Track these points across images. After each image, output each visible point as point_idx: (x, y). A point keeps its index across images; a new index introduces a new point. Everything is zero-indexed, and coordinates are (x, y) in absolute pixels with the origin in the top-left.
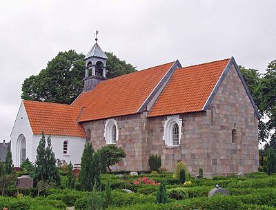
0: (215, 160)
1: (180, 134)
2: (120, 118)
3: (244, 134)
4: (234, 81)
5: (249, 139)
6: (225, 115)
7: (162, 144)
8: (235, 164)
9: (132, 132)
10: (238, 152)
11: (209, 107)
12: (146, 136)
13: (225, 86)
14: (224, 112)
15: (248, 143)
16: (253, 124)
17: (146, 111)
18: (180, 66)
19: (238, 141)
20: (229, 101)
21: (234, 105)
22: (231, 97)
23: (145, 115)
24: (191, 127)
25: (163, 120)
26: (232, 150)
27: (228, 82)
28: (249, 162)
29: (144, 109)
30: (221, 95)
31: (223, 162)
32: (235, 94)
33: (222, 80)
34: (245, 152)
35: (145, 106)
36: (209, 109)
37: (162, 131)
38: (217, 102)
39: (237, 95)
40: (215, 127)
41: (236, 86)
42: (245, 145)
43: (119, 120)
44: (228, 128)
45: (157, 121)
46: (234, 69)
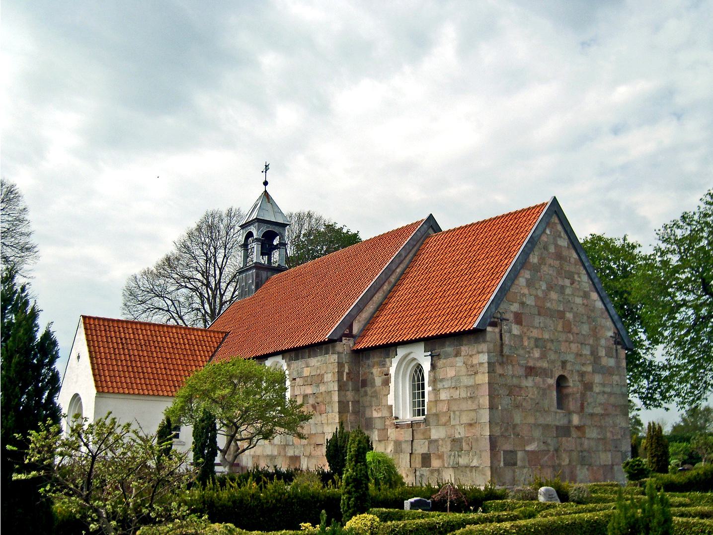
0: (513, 452)
1: (428, 389)
2: (293, 355)
3: (588, 387)
4: (559, 256)
5: (193, 337)
6: (537, 340)
7: (385, 413)
8: (566, 462)
9: (318, 386)
10: (574, 433)
11: (494, 320)
12: (350, 395)
13: (536, 269)
14: (535, 333)
15: (599, 410)
16: (611, 362)
17: (350, 335)
18: (436, 228)
19: (572, 405)
20: (548, 305)
21: (561, 315)
22: (554, 295)
23: (345, 346)
24: (451, 373)
25: (388, 356)
26: (557, 427)
27: (542, 260)
28: (605, 458)
29: (346, 331)
30: (526, 291)
31: (534, 458)
32: (563, 288)
33: (526, 253)
34: (592, 433)
35: (348, 324)
36: (494, 324)
37: (386, 382)
38: (515, 307)
39: (568, 291)
40: (509, 370)
41: (567, 267)
42: (592, 415)
43: (291, 359)
44: (545, 373)
45: (375, 359)
46: (559, 227)
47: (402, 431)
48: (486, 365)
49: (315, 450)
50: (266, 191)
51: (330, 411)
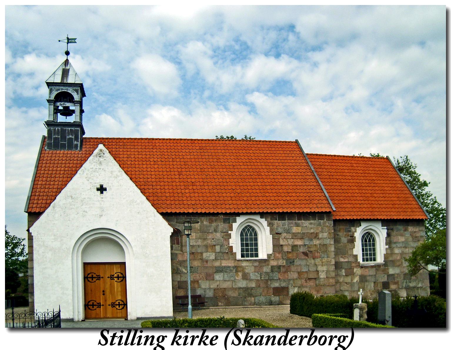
9: (312, 240)
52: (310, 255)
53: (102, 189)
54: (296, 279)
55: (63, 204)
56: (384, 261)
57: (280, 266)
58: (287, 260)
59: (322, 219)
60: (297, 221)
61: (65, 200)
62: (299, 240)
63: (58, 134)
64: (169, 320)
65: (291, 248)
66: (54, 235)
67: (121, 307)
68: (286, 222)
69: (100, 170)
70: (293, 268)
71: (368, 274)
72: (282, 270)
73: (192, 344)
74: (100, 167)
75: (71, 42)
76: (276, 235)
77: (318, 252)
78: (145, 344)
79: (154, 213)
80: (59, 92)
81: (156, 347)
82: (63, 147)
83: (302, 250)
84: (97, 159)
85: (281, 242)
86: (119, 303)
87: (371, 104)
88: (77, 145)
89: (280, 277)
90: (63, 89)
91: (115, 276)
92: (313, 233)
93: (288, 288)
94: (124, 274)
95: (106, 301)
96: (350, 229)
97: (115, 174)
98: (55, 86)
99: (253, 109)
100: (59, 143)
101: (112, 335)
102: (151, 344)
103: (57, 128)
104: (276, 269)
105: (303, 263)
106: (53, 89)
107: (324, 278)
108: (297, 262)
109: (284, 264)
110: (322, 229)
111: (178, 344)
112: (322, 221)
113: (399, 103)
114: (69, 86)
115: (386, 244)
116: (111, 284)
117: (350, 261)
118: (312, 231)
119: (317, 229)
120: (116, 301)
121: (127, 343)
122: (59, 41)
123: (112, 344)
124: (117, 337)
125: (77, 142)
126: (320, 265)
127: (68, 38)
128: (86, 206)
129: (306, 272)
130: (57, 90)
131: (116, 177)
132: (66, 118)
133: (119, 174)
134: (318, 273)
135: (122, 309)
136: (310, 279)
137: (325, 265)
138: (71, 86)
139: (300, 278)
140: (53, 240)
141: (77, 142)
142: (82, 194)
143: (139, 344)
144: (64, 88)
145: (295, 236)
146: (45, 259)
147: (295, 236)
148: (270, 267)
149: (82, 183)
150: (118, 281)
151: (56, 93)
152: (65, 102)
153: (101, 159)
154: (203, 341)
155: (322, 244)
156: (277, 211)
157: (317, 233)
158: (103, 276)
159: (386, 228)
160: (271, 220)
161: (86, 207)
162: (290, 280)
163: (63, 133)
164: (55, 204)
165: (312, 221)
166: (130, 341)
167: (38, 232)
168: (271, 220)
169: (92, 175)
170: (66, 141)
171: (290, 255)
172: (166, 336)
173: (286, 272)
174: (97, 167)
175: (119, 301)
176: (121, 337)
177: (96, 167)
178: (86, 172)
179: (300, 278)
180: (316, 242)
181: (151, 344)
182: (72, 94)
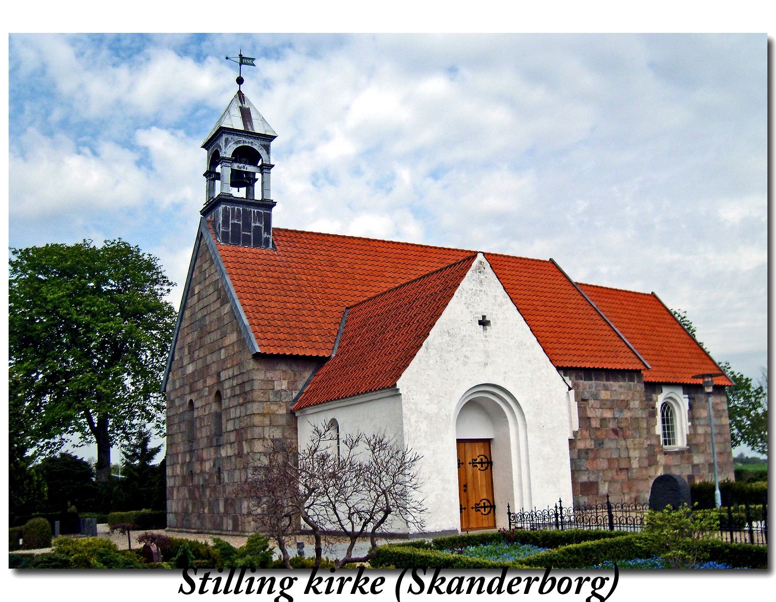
9: (621, 411)
47: (671, 457)
48: (727, 411)
49: (617, 474)
50: (240, 92)
51: (638, 436)
52: (620, 433)
53: (484, 323)
54: (607, 470)
55: (440, 343)
56: (687, 445)
57: (589, 449)
58: (595, 441)
59: (631, 380)
60: (605, 383)
61: (440, 338)
62: (608, 410)
63: (238, 218)
64: (107, 559)
65: (599, 422)
66: (430, 394)
67: (487, 510)
68: (593, 382)
69: (481, 293)
70: (603, 454)
71: (673, 464)
72: (591, 455)
73: (339, 592)
74: (481, 288)
75: (245, 64)
76: (582, 402)
77: (629, 430)
78: (259, 592)
79: (546, 362)
80: (239, 145)
81: (279, 597)
82: (247, 241)
83: (612, 425)
84: (476, 275)
85: (590, 413)
86: (484, 503)
87: (357, 172)
88: (267, 240)
89: (588, 467)
90: (246, 142)
91: (477, 461)
92: (624, 400)
93: (597, 483)
94: (488, 457)
95: (468, 501)
96: (652, 396)
97: (499, 300)
98: (234, 134)
99: (145, 160)
100: (240, 233)
101: (203, 577)
102: (270, 591)
103: (236, 208)
104: (583, 455)
105: (612, 445)
106: (230, 139)
107: (637, 468)
108: (609, 444)
109: (593, 447)
110: (633, 394)
111: (316, 592)
112: (632, 383)
113: (405, 175)
114: (255, 138)
115: (689, 421)
116: (473, 474)
117: (652, 443)
118: (622, 397)
119: (628, 395)
120: (481, 501)
121: (229, 591)
122: (227, 58)
123: (201, 591)
124: (211, 579)
125: (267, 234)
126: (632, 448)
127: (241, 55)
128: (468, 348)
129: (616, 458)
130: (237, 143)
131: (501, 305)
132: (238, 191)
133: (504, 301)
134: (630, 461)
135: (488, 514)
136: (621, 469)
137: (637, 449)
138: (258, 139)
139: (610, 468)
140: (428, 402)
141: (267, 234)
142: (462, 329)
143: (248, 591)
144: (247, 140)
145: (603, 404)
146: (419, 433)
147: (603, 404)
148: (576, 451)
149: (461, 311)
150: (482, 469)
151: (235, 147)
152: (246, 163)
153: (482, 277)
154: (313, 587)
155: (634, 417)
156: (583, 365)
157: (627, 401)
158: (463, 462)
159: (687, 396)
160: (576, 379)
161: (467, 351)
162: (599, 471)
163: (246, 216)
164: (428, 342)
165: (622, 383)
166: (233, 586)
167: (407, 389)
168: (576, 379)
169: (472, 300)
170: (250, 232)
171: (599, 433)
172: (296, 579)
173: (595, 459)
174: (478, 288)
175: (484, 501)
176: (219, 580)
177: (476, 288)
178: (465, 295)
179: (610, 468)
180: (627, 414)
181: (270, 591)
182: (260, 152)
